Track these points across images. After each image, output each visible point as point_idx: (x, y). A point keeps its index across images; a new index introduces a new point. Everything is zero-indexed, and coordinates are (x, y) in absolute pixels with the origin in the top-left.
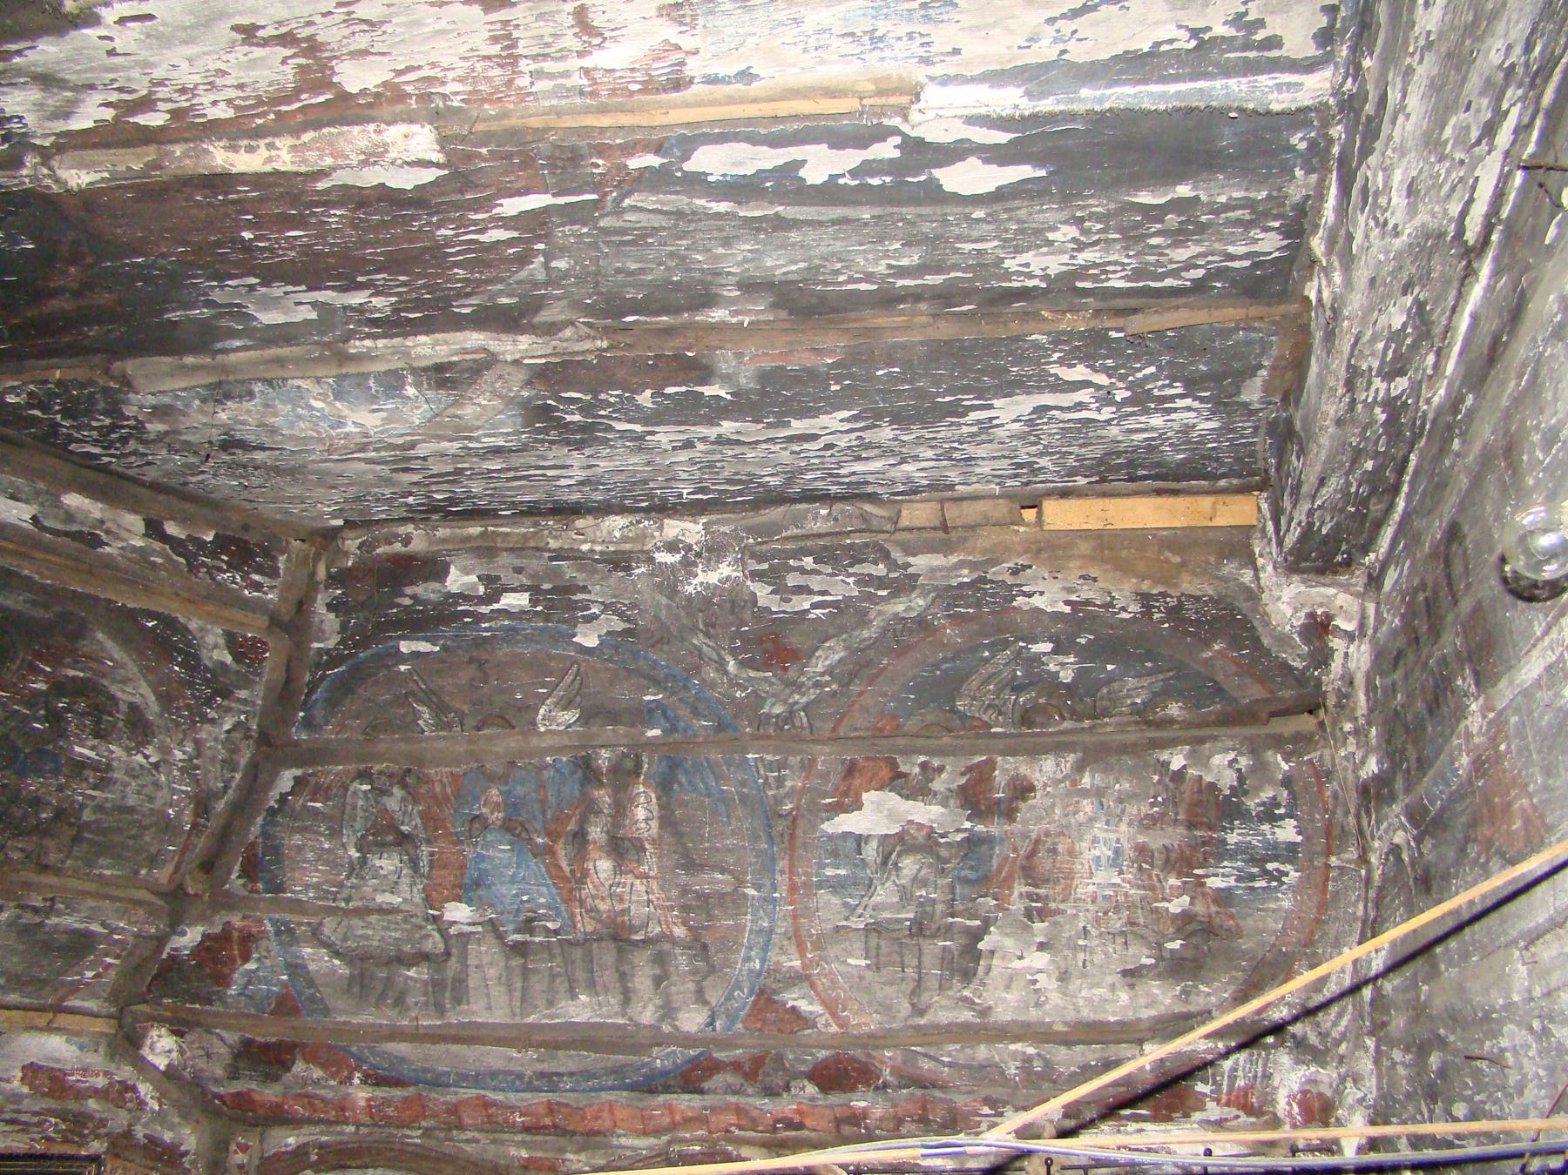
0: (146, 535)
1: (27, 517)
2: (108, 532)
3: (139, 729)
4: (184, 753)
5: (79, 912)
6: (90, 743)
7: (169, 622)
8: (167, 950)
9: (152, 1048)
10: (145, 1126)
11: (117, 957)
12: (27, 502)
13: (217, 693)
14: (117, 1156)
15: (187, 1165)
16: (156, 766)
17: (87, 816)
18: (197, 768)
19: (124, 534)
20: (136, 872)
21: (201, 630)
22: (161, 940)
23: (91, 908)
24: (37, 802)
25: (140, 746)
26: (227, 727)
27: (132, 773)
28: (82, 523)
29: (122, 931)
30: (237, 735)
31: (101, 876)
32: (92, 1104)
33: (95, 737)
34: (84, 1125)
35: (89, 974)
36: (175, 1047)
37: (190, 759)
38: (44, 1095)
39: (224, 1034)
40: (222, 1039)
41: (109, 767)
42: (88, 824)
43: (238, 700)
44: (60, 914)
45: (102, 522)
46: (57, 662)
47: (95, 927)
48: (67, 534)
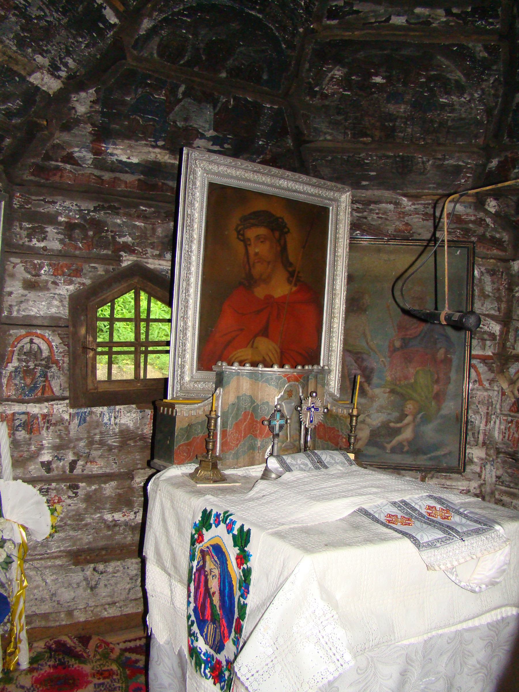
0: (446, 16)
1: (404, 21)
2: (433, 18)
3: (461, 89)
4: (478, 94)
5: (454, 158)
6: (445, 97)
7: (461, 46)
8: (487, 169)
9: (488, 205)
10: (489, 232)
11: (471, 173)
12: (403, 16)
13: (485, 69)
14: (480, 242)
15: (505, 246)
16: (469, 101)
17: (450, 123)
18: (484, 99)
19: (438, 17)
20: (471, 142)
21: (473, 46)
22: (485, 165)
23: (458, 157)
24: (432, 121)
25: (462, 95)
26: (491, 82)
27: (462, 105)
28: (423, 18)
29: (470, 164)
30: (496, 84)
31: (459, 145)
32: (471, 225)
33: (446, 94)
34: (469, 232)
35: (463, 181)
36: (496, 204)
37: (481, 96)
38: (455, 223)
39: (512, 198)
40: (511, 199)
41: (453, 105)
42: (450, 126)
43: (493, 70)
44: (448, 160)
45: (430, 15)
46: (427, 70)
47: (461, 163)
48: (419, 23)
